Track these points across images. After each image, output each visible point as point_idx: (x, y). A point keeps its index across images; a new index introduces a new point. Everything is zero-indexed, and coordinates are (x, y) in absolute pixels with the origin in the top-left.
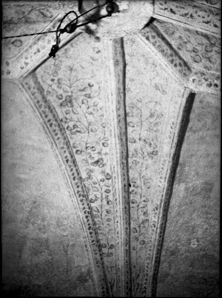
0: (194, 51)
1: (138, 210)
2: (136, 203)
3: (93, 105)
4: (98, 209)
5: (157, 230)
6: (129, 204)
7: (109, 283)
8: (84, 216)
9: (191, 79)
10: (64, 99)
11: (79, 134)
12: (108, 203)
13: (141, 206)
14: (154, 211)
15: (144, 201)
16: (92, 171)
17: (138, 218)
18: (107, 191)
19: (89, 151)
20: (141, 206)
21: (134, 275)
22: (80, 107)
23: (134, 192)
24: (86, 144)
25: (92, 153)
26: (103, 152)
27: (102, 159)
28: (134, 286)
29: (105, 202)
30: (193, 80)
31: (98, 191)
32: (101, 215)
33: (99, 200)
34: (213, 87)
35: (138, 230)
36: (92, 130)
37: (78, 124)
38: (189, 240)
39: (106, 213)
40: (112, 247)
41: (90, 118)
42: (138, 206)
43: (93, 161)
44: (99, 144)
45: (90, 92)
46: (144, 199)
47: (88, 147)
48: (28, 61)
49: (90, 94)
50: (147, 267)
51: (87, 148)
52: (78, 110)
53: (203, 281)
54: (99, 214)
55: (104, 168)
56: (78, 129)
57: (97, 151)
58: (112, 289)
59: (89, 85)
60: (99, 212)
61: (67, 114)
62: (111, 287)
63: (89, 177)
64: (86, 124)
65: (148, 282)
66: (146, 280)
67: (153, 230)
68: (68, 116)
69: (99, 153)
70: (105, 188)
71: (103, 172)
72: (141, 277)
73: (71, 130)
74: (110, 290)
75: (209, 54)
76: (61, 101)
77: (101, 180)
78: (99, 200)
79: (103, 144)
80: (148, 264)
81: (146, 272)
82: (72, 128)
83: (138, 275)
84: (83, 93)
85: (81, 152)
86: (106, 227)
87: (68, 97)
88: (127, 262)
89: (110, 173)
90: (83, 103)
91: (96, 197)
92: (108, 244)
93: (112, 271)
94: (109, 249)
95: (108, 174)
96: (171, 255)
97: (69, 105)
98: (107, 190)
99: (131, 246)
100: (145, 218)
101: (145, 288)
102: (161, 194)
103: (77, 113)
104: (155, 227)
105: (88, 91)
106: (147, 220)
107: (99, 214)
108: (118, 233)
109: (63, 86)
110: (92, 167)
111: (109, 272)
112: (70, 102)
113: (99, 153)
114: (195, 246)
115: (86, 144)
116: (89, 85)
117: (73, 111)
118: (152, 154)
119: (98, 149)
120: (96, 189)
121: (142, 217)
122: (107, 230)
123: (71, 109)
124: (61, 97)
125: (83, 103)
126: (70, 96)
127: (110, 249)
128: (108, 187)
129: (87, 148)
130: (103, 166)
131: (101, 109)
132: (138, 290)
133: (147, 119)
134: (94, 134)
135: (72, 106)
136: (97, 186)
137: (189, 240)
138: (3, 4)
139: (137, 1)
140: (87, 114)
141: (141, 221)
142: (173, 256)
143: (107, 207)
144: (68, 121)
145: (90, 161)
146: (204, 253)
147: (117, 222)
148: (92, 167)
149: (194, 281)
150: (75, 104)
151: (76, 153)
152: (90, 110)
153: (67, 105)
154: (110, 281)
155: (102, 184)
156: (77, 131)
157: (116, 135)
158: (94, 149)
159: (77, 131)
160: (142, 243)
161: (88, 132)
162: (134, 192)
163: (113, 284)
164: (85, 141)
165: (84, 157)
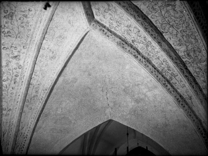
0: (98, 9)
1: (33, 89)
2: (33, 85)
3: (26, 22)
4: (7, 86)
5: (43, 102)
6: (29, 85)
7: (2, 132)
9: (92, 24)
10: (8, 14)
11: (9, 37)
12: (15, 83)
13: (35, 87)
14: (44, 91)
15: (38, 84)
16: (10, 62)
17: (32, 94)
18: (16, 76)
19: (13, 49)
20: (35, 87)
21: (20, 128)
22: (17, 21)
23: (34, 79)
24: (12, 44)
25: (14, 51)
26: (22, 52)
27: (19, 56)
28: (19, 134)
29: (13, 82)
30: (93, 25)
31: (10, 75)
32: (8, 90)
33: (9, 81)
34: (102, 31)
35: (29, 101)
36: (19, 37)
38: (57, 108)
39: (11, 89)
40: (10, 110)
42: (34, 87)
43: (12, 56)
44: (21, 46)
45: (27, 14)
46: (39, 83)
47: (13, 46)
49: (27, 15)
50: (31, 123)
51: (11, 47)
52: (15, 22)
53: (60, 131)
54: (7, 89)
55: (19, 61)
56: (10, 34)
57: (17, 50)
58: (3, 136)
59: (29, 10)
60: (7, 88)
61: (6, 23)
62: (3, 135)
63: (7, 65)
64: (17, 32)
65: (29, 132)
66: (29, 130)
67: (40, 102)
68: (6, 25)
69: (19, 52)
70: (15, 74)
71: (17, 64)
72: (24, 129)
73: (4, 34)
74: (3, 137)
76: (5, 14)
77: (14, 68)
78: (9, 81)
79: (23, 47)
80: (32, 121)
81: (29, 126)
82: (6, 33)
83: (23, 128)
84: (23, 13)
85: (7, 48)
86: (9, 98)
87: (11, 13)
88: (19, 120)
89: (22, 65)
90: (20, 19)
91: (8, 79)
92: (8, 108)
93: (6, 125)
94: (7, 112)
95: (20, 65)
96: (45, 116)
97: (10, 18)
98: (16, 75)
99: (23, 110)
100: (36, 94)
101: (27, 135)
102: (51, 82)
103: (13, 24)
104: (42, 100)
106: (37, 95)
107: (7, 89)
108: (17, 102)
110: (11, 59)
111: (4, 125)
112: (12, 16)
113: (19, 52)
114: (60, 112)
115: (12, 44)
116: (29, 10)
117: (11, 22)
118: (52, 58)
119: (19, 49)
120: (9, 73)
121: (34, 94)
122: (9, 99)
123: (10, 21)
124: (6, 12)
126: (13, 13)
127: (8, 112)
128: (18, 73)
129: (11, 47)
130: (19, 60)
131: (30, 25)
132: (21, 136)
133: (57, 38)
134: (19, 39)
135: (12, 19)
136: (11, 72)
137: (57, 108)
140: (20, 27)
141: (33, 95)
142: (46, 117)
143: (13, 85)
144: (5, 28)
145: (11, 55)
146: (64, 116)
147: (19, 95)
149: (55, 131)
150: (14, 18)
151: (3, 49)
152: (23, 24)
153: (9, 18)
154: (3, 131)
155: (14, 71)
156: (9, 36)
157: (37, 44)
158: (16, 48)
159: (9, 36)
160: (30, 108)
161: (16, 38)
162: (34, 79)
163: (5, 133)
164: (12, 42)
165: (8, 53)
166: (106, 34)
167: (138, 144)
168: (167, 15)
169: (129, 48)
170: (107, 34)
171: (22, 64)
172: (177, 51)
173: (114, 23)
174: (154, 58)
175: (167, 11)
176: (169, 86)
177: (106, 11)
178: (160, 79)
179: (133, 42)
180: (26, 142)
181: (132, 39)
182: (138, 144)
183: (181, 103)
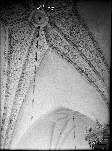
8: (7, 80)
16: (13, 66)
37: (15, 50)
41: (19, 49)
48: (14, 24)
70: (15, 73)
75: (54, 41)
76: (14, 41)
79: (20, 59)
84: (21, 41)
90: (19, 44)
105: (22, 41)
109: (17, 37)
112: (16, 42)
123: (15, 44)
125: (19, 44)
135: (16, 43)
138: (2, 148)
139: (84, 10)
148: (14, 65)
152: (20, 47)
166: (55, 50)
167: (75, 147)
168: (78, 38)
169: (65, 57)
170: (56, 50)
171: (18, 68)
172: (85, 56)
173: (58, 45)
174: (77, 62)
175: (78, 36)
176: (85, 75)
177: (55, 39)
178: (81, 72)
179: (67, 55)
180: (16, 115)
181: (67, 53)
182: (75, 147)
183: (91, 83)
